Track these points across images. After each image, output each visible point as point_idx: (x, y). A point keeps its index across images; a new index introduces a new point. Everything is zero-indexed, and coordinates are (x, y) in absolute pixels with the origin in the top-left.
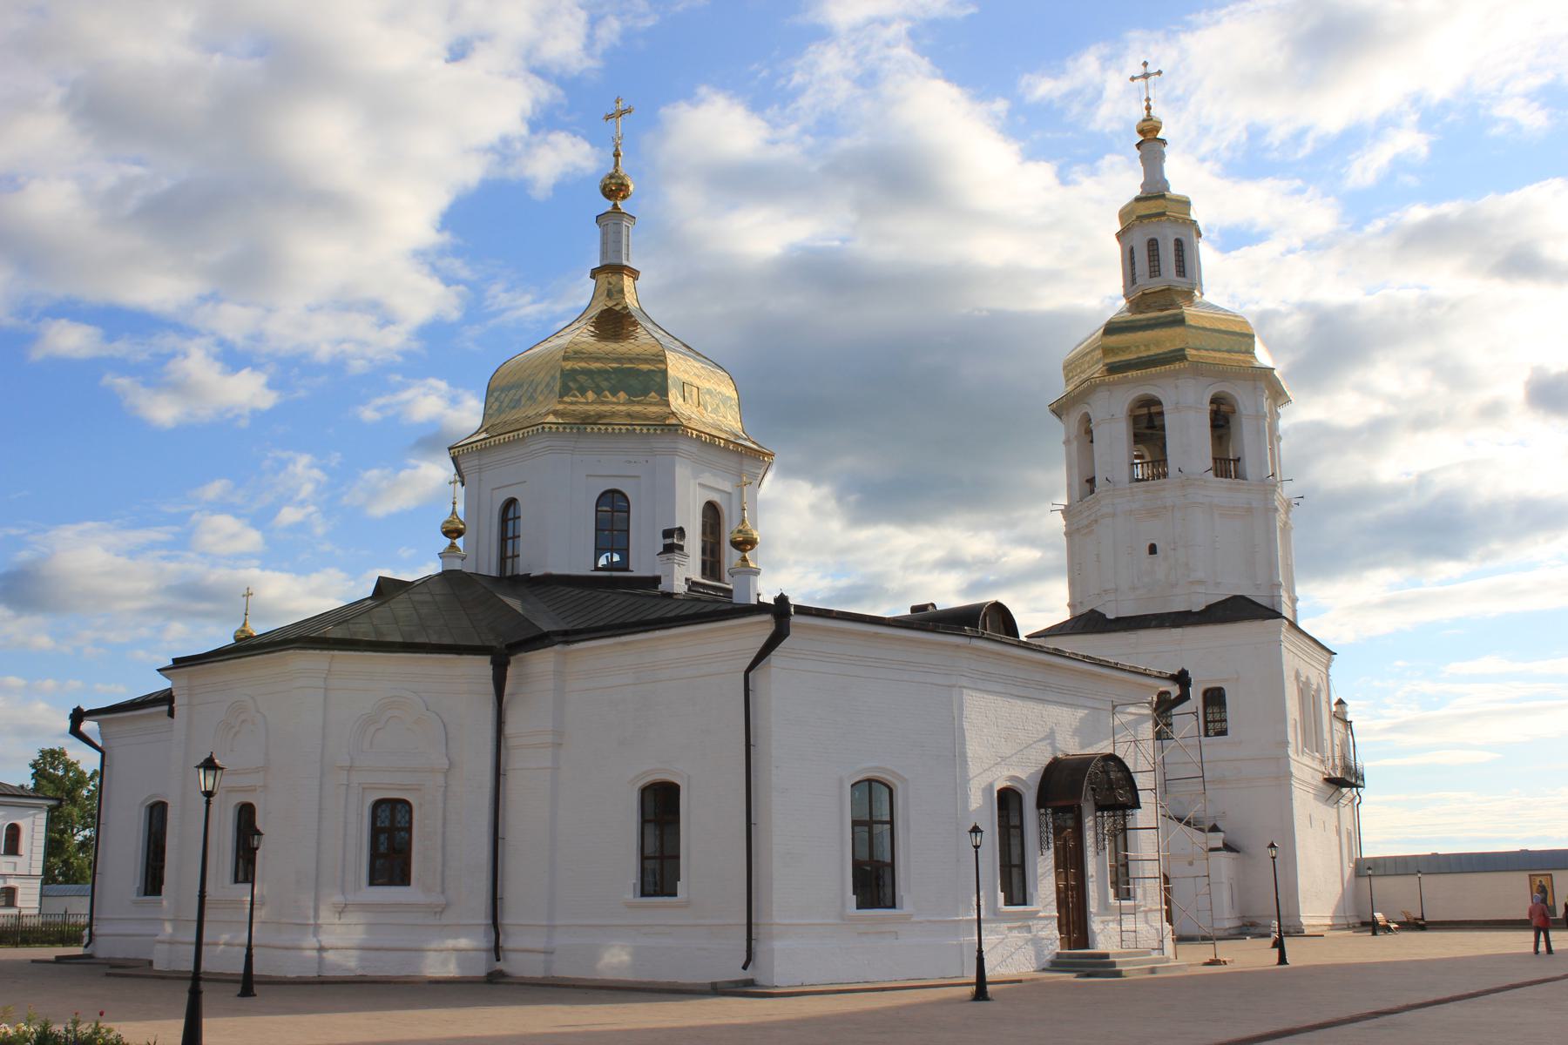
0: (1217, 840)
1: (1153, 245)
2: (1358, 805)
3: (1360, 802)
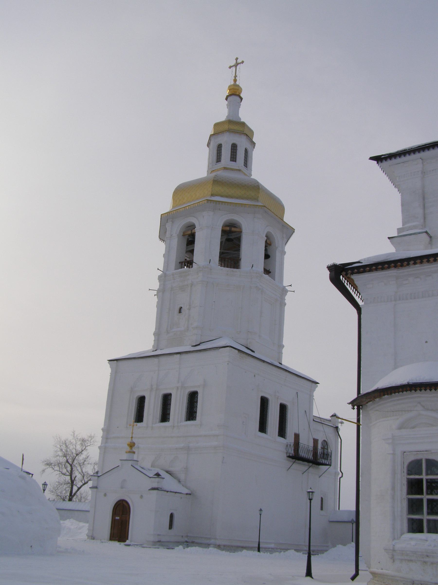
1: (220, 147)
2: (340, 478)
3: (342, 476)
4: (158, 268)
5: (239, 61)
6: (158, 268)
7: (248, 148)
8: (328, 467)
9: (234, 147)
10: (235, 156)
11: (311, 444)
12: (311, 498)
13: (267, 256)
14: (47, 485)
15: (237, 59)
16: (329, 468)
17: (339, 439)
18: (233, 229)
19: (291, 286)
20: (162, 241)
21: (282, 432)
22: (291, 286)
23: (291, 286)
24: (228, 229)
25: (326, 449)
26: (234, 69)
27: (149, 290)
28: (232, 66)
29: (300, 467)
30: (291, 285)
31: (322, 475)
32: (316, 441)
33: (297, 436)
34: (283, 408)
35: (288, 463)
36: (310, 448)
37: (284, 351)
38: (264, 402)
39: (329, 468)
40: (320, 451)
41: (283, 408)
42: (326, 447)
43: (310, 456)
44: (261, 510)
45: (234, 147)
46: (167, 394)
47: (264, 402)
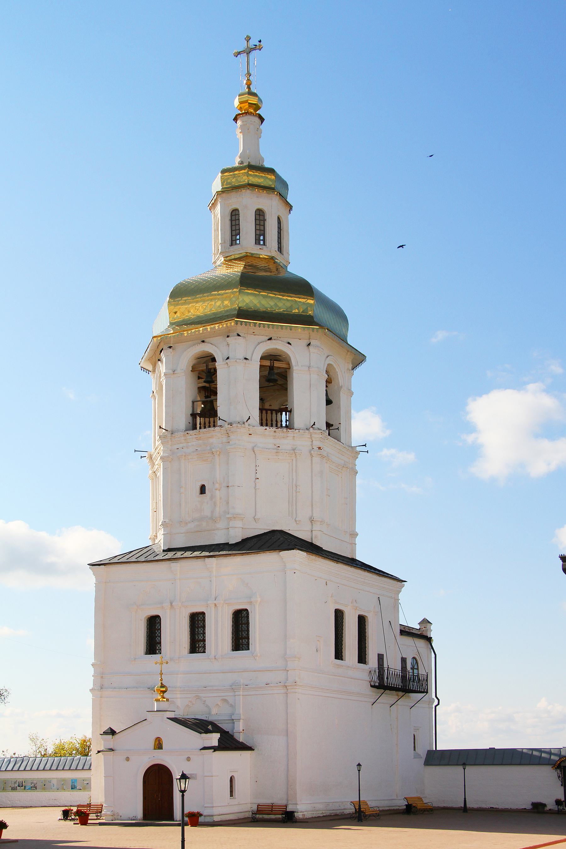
0: (214, 739)
2: (436, 706)
3: (438, 704)
4: (160, 426)
5: (252, 43)
6: (160, 426)
7: (282, 216)
8: (421, 695)
9: (260, 215)
10: (257, 223)
11: (399, 667)
12: (183, 789)
13: (329, 402)
14: (361, 765)
15: (248, 39)
16: (405, 694)
17: (433, 653)
18: (277, 364)
19: (365, 445)
20: (144, 371)
21: (362, 658)
22: (365, 445)
23: (366, 447)
24: (267, 363)
25: (416, 669)
26: (244, 57)
27: (135, 451)
28: (239, 53)
29: (388, 698)
30: (366, 444)
31: (414, 705)
32: (404, 660)
33: (380, 657)
34: (362, 621)
35: (373, 694)
36: (397, 672)
37: (358, 540)
38: (339, 615)
39: (405, 694)
40: (424, 677)
41: (362, 621)
42: (416, 667)
43: (397, 682)
44: (359, 765)
45: (260, 215)
46: (196, 612)
47: (339, 615)
